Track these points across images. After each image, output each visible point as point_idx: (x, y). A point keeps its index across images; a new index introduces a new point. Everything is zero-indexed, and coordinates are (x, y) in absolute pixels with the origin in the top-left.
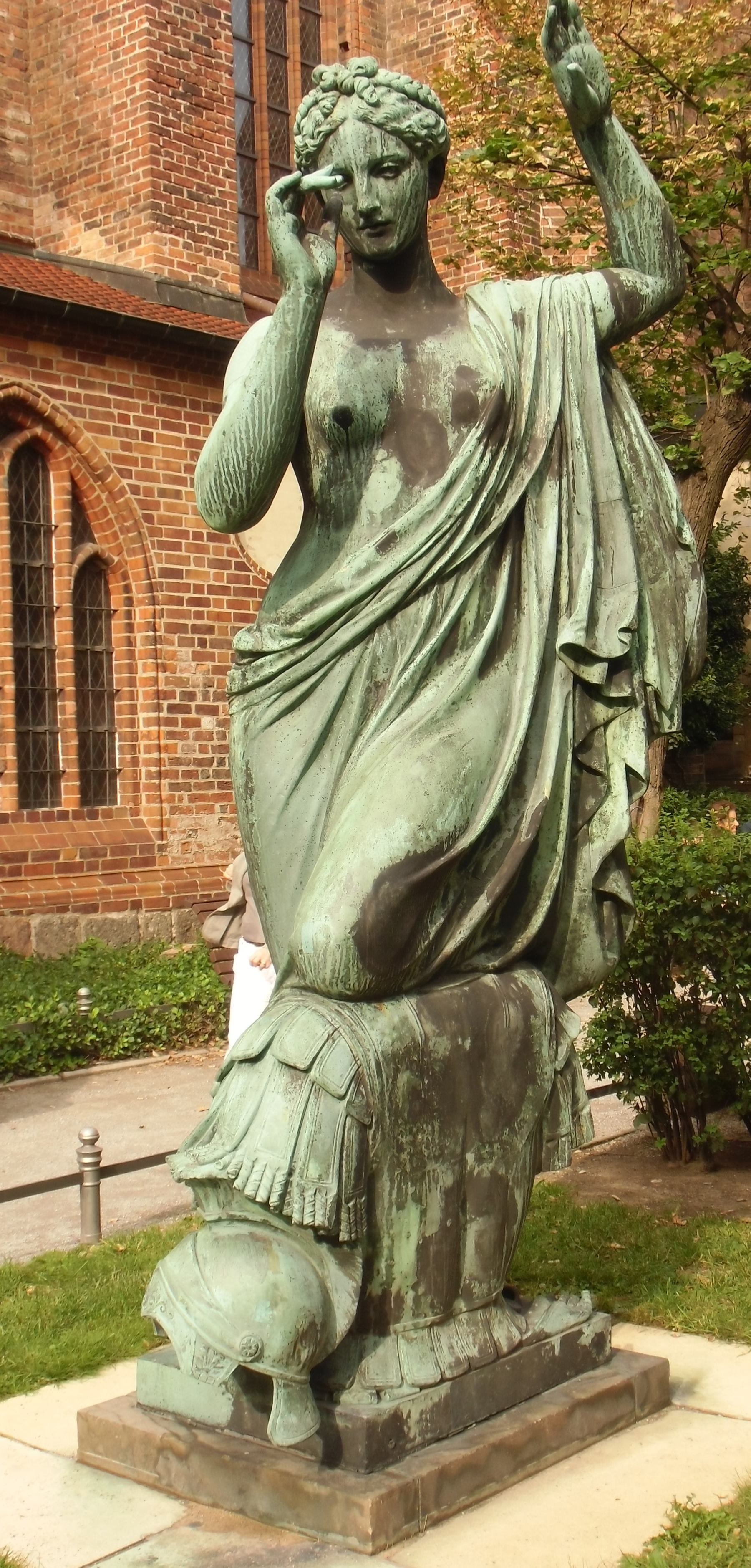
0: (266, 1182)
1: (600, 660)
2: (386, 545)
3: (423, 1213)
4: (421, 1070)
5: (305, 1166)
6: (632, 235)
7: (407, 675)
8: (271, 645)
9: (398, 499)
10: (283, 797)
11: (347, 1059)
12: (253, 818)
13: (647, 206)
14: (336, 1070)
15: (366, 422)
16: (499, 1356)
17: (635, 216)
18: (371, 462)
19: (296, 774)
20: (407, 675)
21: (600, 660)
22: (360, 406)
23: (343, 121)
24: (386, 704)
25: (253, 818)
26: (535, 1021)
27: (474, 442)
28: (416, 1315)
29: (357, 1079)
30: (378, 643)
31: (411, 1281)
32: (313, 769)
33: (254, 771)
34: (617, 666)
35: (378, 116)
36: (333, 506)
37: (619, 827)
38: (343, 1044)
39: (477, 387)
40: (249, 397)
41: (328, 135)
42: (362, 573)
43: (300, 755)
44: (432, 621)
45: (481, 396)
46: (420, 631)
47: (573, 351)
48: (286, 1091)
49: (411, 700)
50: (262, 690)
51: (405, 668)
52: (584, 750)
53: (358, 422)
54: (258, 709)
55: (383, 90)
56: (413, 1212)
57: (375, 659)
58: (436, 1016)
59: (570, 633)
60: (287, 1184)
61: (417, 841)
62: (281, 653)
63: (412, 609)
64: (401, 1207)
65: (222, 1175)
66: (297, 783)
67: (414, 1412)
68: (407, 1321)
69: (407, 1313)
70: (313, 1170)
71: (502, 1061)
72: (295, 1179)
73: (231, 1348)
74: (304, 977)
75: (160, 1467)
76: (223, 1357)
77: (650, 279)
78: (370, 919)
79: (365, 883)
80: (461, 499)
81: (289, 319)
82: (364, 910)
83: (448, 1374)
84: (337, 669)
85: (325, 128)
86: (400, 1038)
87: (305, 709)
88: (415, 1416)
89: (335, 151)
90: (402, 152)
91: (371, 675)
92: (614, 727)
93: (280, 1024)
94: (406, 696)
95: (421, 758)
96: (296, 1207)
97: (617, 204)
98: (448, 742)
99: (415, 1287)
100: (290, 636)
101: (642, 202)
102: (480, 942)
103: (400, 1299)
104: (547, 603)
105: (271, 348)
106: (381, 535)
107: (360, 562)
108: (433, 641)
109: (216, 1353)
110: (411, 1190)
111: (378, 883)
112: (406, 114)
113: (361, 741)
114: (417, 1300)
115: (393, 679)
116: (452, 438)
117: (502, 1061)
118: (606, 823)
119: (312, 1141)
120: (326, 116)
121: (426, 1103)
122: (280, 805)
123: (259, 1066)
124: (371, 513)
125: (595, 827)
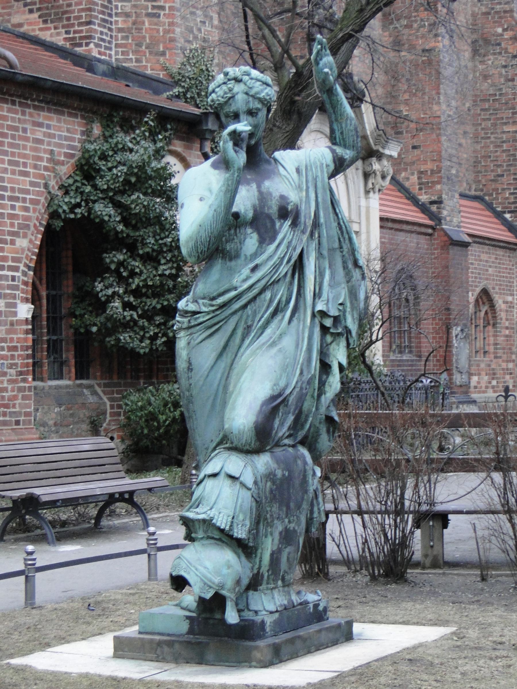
0: (224, 521)
1: (330, 316)
2: (254, 269)
3: (273, 540)
4: (274, 482)
5: (238, 516)
6: (342, 133)
7: (261, 323)
8: (204, 309)
9: (257, 250)
10: (206, 373)
11: (252, 475)
12: (191, 381)
13: (349, 122)
14: (248, 479)
15: (245, 218)
16: (294, 606)
17: (344, 125)
18: (246, 234)
19: (212, 363)
20: (261, 323)
21: (330, 316)
22: (243, 211)
23: (237, 93)
24: (253, 334)
25: (191, 381)
26: (307, 468)
27: (287, 227)
28: (268, 583)
29: (255, 483)
30: (249, 310)
31: (267, 568)
32: (219, 362)
33: (193, 361)
34: (336, 320)
35: (252, 92)
36: (228, 252)
37: (336, 388)
38: (249, 469)
39: (288, 204)
40: (212, 212)
41: (230, 98)
42: (245, 280)
43: (214, 355)
44: (271, 301)
45: (290, 208)
46: (266, 304)
47: (319, 185)
48: (230, 486)
49: (262, 333)
50: (198, 328)
51: (259, 321)
52: (323, 354)
53: (242, 218)
54: (195, 336)
55: (253, 81)
56: (269, 540)
57: (248, 316)
58: (278, 461)
59: (320, 306)
60: (232, 522)
61: (273, 390)
62: (208, 313)
63: (263, 296)
64: (266, 537)
65: (208, 518)
66: (212, 367)
67: (269, 620)
68: (264, 586)
69: (265, 582)
70: (241, 517)
71: (297, 482)
72: (235, 520)
73: (214, 583)
74: (232, 443)
75: (158, 652)
76: (211, 587)
77: (348, 152)
78: (260, 420)
79: (257, 406)
80: (282, 251)
81: (230, 183)
82: (257, 417)
83: (279, 609)
84: (231, 320)
85: (229, 95)
86: (267, 469)
87: (216, 337)
88: (268, 624)
89: (233, 105)
90: (259, 106)
91: (246, 323)
92: (334, 344)
93: (225, 461)
94: (260, 331)
95: (271, 357)
96: (235, 530)
97: (336, 120)
98: (280, 350)
99: (268, 571)
100: (212, 306)
101: (347, 119)
102: (287, 434)
103: (263, 576)
104: (312, 294)
105: (222, 194)
106: (252, 265)
107: (243, 277)
108: (271, 309)
109: (208, 586)
110: (269, 530)
111: (262, 405)
112: (262, 91)
113: (242, 350)
114: (268, 576)
115: (255, 324)
116: (278, 225)
117: (297, 482)
118: (331, 386)
119: (241, 506)
120: (230, 91)
121: (275, 496)
122: (205, 376)
123: (217, 477)
124: (245, 255)
125: (327, 388)
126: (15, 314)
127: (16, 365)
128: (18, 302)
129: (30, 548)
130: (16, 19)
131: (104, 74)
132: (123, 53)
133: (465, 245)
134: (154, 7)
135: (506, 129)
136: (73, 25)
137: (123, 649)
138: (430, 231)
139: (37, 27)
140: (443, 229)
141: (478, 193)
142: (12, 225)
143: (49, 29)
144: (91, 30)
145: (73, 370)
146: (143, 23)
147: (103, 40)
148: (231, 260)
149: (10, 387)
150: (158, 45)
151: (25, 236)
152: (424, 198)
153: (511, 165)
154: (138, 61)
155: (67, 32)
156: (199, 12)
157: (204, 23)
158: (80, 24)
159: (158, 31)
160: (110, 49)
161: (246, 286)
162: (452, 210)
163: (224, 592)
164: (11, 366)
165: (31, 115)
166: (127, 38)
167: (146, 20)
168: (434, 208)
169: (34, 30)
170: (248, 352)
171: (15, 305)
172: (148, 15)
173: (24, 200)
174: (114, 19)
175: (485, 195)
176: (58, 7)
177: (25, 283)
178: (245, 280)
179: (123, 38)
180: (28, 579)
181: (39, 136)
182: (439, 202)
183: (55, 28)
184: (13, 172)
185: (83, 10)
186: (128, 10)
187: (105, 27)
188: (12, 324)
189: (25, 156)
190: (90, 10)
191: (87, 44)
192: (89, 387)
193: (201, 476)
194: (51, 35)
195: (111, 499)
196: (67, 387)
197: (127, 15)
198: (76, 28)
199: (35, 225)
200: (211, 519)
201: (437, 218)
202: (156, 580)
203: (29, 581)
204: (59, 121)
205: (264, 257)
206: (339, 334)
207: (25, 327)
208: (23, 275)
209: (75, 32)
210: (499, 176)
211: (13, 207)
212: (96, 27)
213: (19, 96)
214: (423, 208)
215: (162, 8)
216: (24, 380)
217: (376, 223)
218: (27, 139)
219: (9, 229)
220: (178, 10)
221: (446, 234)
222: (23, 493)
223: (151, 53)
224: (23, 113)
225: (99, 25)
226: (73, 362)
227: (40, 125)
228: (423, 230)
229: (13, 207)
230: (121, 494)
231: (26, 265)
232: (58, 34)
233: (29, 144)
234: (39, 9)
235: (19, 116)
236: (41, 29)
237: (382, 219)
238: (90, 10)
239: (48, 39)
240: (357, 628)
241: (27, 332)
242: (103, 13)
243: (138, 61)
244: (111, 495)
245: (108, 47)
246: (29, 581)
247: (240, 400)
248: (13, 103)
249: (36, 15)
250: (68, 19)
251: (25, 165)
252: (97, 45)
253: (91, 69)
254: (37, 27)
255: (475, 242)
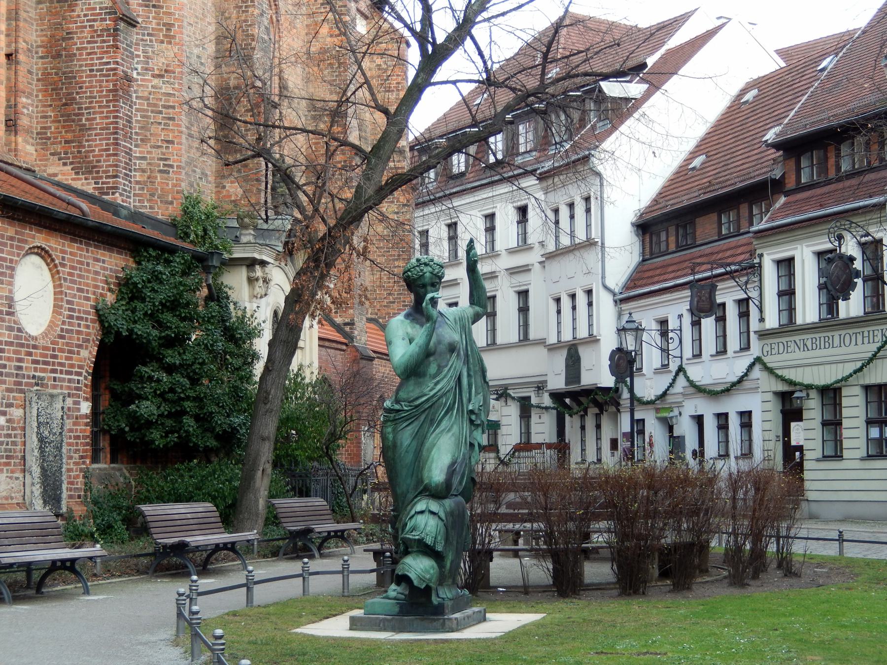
8: (405, 408)
59: (470, 408)
78: (252, 496)
126: (79, 410)
127: (79, 450)
128: (81, 400)
129: (306, 560)
130: (51, 170)
131: (126, 218)
132: (139, 201)
133: (371, 359)
134: (165, 165)
135: (396, 263)
136: (101, 177)
137: (355, 624)
138: (344, 347)
139: (70, 178)
140: (354, 346)
141: (373, 316)
142: (78, 339)
143: (81, 179)
144: (117, 182)
145: (109, 456)
146: (156, 177)
147: (125, 190)
148: (420, 377)
149: (75, 468)
150: (168, 196)
151: (87, 348)
152: (338, 320)
153: (401, 294)
154: (151, 208)
155: (95, 183)
156: (198, 170)
157: (201, 179)
158: (107, 177)
159: (167, 184)
160: (129, 197)
161: (432, 393)
162: (361, 331)
163: (431, 584)
164: (76, 451)
165: (92, 253)
166: (143, 189)
167: (158, 175)
168: (347, 329)
169: (67, 180)
170: (433, 435)
171: (78, 403)
172: (160, 171)
173: (87, 320)
174: (133, 173)
175: (380, 318)
176: (89, 162)
177: (86, 386)
178: (431, 390)
179: (139, 189)
180: (248, 589)
181: (98, 269)
182: (351, 324)
183: (86, 179)
184: (80, 298)
185: (110, 166)
186: (144, 167)
187: (126, 180)
188: (77, 418)
189: (87, 285)
190: (116, 166)
191: (113, 194)
192: (120, 470)
193: (413, 512)
194: (82, 185)
195: (217, 548)
196: (105, 469)
197: (143, 171)
198: (104, 180)
199: (93, 340)
200: (423, 539)
201: (350, 337)
202: (252, 606)
203: (249, 590)
204: (110, 257)
205: (441, 376)
206: (478, 425)
207: (85, 421)
208: (85, 380)
209: (103, 183)
210: (391, 302)
211: (79, 325)
212: (121, 180)
213: (85, 238)
214: (338, 328)
215: (171, 166)
216: (84, 463)
217: (316, 342)
218: (88, 271)
219: (7, 339)
220: (184, 169)
221: (357, 350)
222: (177, 540)
223: (161, 202)
224: (88, 251)
225: (123, 178)
226: (108, 449)
227: (98, 260)
228: (339, 346)
229: (79, 325)
230: (225, 544)
231: (87, 371)
232: (88, 184)
233: (91, 275)
234: (71, 163)
235: (84, 253)
236: (73, 179)
237: (320, 339)
238: (116, 166)
239: (80, 187)
240: (488, 615)
241: (86, 424)
242: (125, 169)
243: (151, 208)
244: (217, 545)
245: (131, 197)
246: (249, 590)
247: (434, 465)
248: (81, 243)
249: (69, 167)
250: (98, 172)
251: (88, 291)
252: (121, 195)
253: (116, 213)
254: (70, 178)
255: (378, 358)
